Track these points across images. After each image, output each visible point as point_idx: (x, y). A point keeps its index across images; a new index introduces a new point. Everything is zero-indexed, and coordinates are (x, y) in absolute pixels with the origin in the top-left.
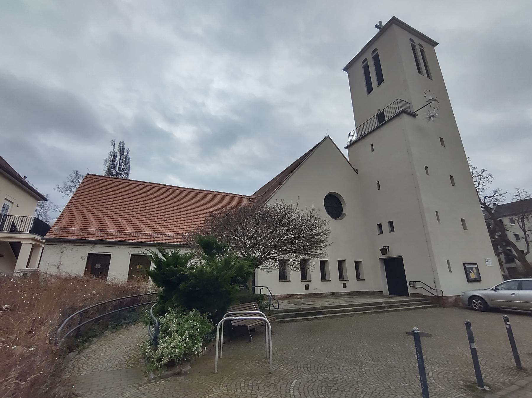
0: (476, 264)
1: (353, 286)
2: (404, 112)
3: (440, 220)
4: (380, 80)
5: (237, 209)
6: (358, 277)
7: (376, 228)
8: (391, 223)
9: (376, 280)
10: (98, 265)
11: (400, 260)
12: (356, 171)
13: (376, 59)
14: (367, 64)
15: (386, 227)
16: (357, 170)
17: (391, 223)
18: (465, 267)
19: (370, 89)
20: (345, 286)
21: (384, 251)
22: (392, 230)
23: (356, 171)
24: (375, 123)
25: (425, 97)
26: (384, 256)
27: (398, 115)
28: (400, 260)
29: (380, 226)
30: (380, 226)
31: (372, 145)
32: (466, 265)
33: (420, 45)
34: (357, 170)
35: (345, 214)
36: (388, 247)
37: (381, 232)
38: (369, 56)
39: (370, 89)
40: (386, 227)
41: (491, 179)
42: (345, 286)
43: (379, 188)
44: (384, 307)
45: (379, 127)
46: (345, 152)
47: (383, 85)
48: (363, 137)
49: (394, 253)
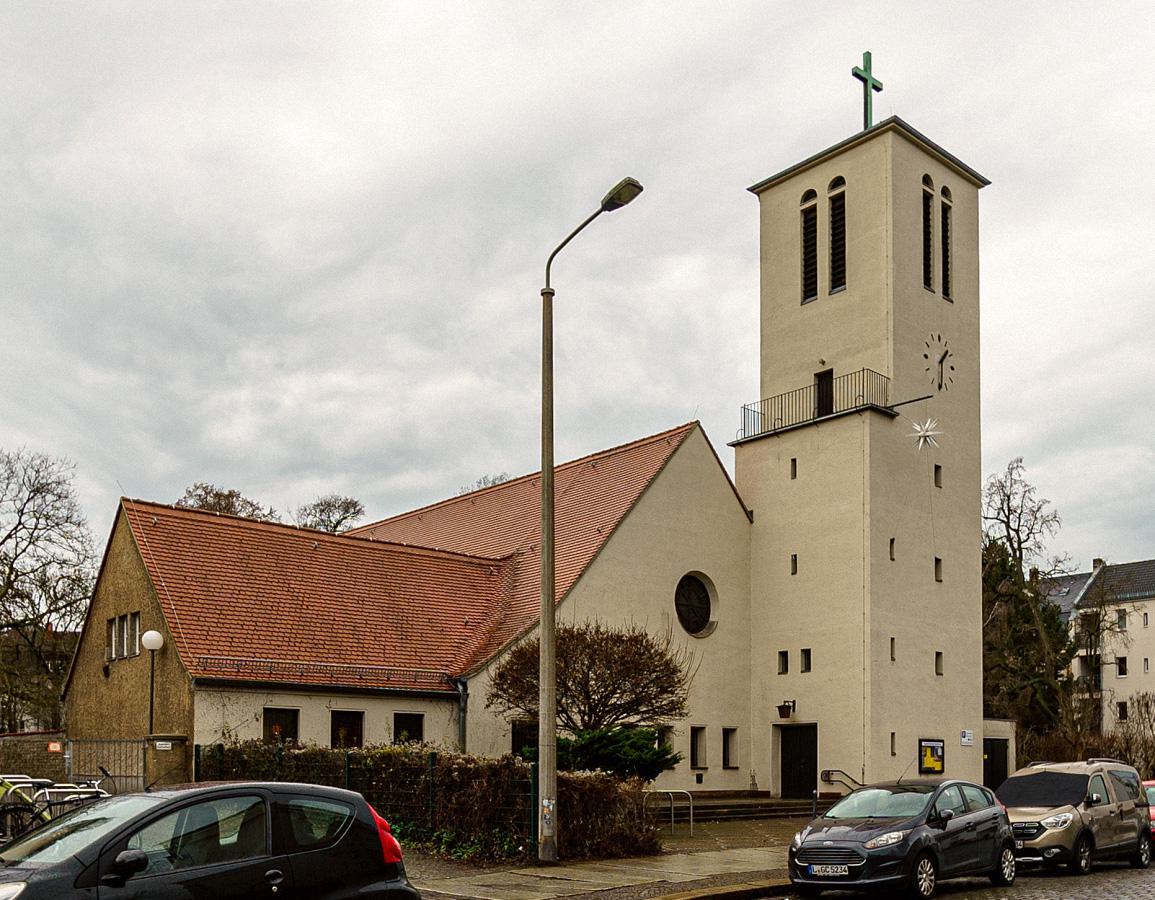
0: (942, 741)
1: (717, 780)
2: (873, 409)
3: (943, 577)
4: (838, 279)
5: (565, 630)
6: (726, 765)
7: (775, 663)
8: (807, 653)
9: (761, 767)
10: (282, 723)
11: (812, 729)
12: (750, 515)
13: (838, 205)
14: (813, 209)
15: (796, 661)
16: (752, 512)
17: (807, 653)
18: (920, 746)
19: (810, 290)
20: (699, 779)
21: (785, 710)
22: (807, 667)
23: (750, 515)
24: (807, 408)
25: (926, 356)
26: (783, 721)
27: (859, 411)
28: (812, 729)
29: (784, 655)
30: (784, 655)
31: (794, 461)
32: (923, 744)
33: (945, 192)
34: (752, 512)
35: (712, 627)
36: (794, 702)
37: (784, 669)
38: (819, 180)
39: (810, 290)
40: (796, 661)
41: (1055, 525)
42: (699, 779)
43: (794, 572)
44: (775, 811)
45: (816, 424)
46: (728, 458)
47: (840, 297)
48: (776, 434)
49: (802, 716)
